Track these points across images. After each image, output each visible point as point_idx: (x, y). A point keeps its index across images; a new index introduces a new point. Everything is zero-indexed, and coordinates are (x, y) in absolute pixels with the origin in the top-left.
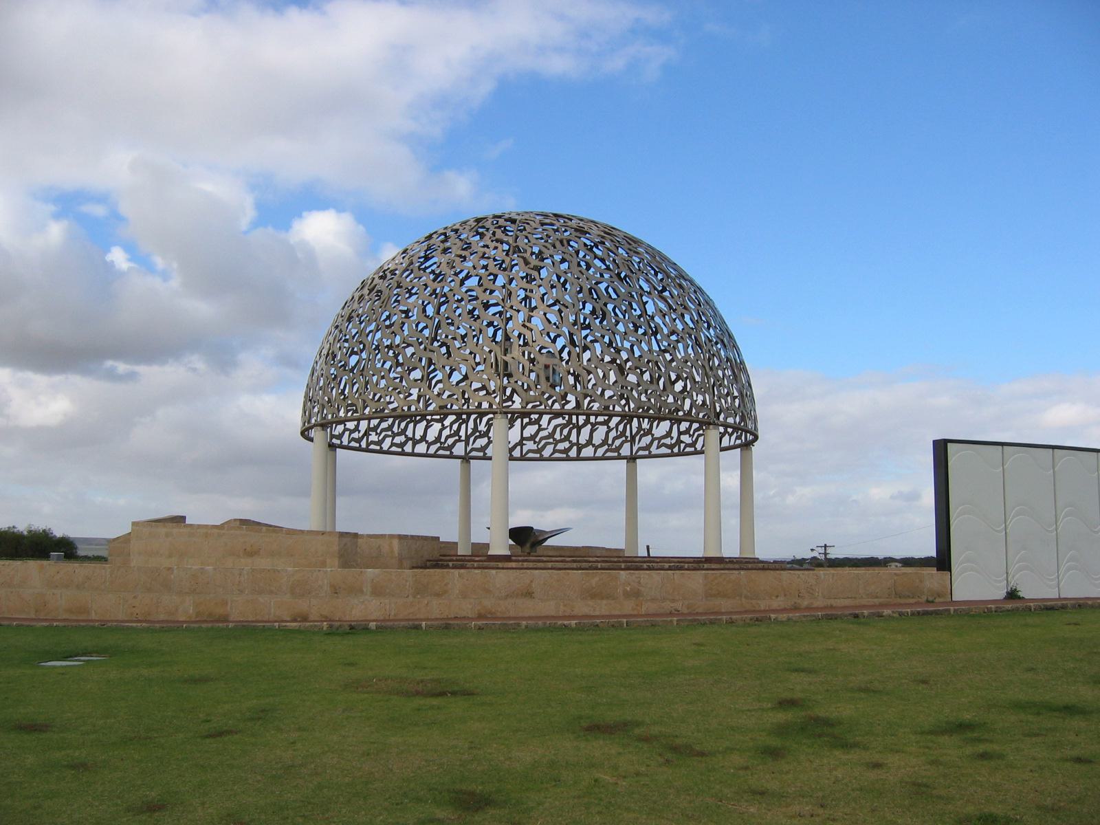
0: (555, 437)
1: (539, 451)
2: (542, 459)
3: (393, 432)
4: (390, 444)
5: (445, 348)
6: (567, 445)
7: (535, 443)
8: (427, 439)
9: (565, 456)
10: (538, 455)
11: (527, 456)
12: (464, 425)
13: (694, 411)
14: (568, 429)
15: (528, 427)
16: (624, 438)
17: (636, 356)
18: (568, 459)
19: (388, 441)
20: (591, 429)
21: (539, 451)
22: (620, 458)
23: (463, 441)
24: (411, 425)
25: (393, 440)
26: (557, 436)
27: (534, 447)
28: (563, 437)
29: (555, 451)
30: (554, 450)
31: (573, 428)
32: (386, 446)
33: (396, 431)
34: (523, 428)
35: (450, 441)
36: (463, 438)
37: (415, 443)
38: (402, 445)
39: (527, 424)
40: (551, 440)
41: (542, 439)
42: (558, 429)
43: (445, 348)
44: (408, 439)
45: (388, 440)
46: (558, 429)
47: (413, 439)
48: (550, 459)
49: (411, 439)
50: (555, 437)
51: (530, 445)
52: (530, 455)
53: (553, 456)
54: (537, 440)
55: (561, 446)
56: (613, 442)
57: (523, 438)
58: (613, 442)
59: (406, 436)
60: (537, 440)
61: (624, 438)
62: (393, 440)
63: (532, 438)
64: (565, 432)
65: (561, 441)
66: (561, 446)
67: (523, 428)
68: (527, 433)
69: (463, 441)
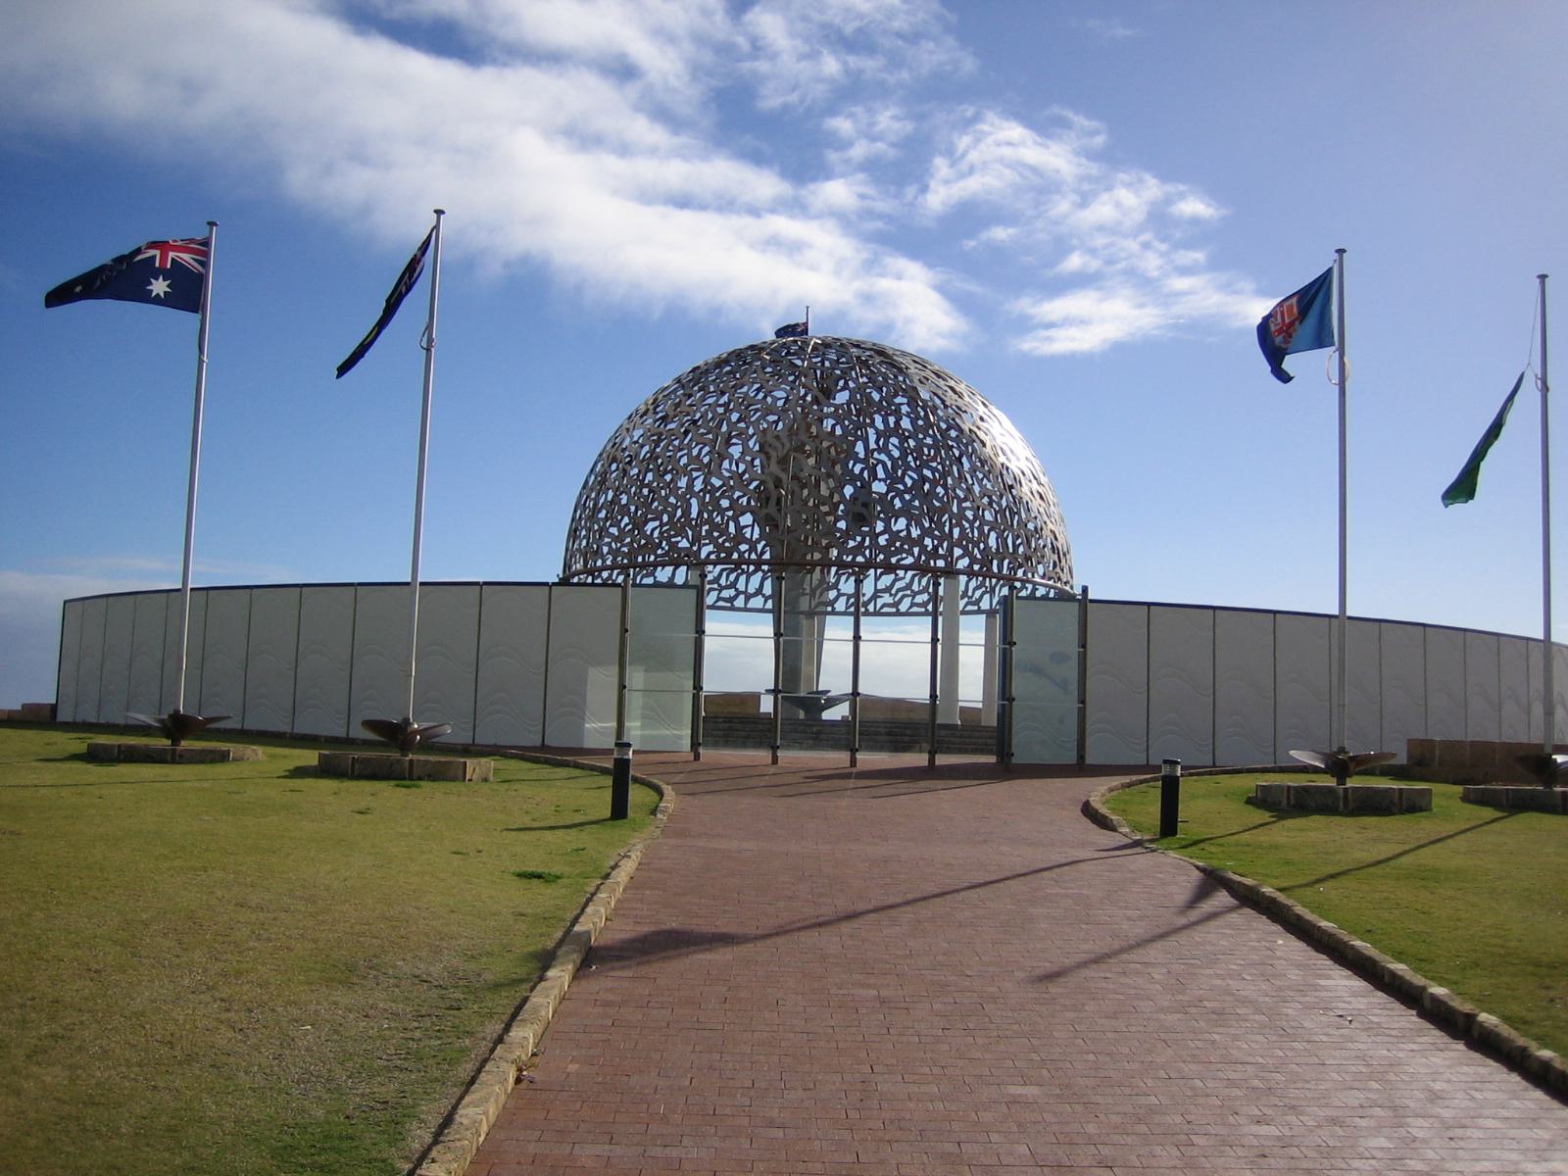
0: (913, 588)
1: (896, 605)
2: (898, 614)
3: (719, 585)
4: (909, 604)
5: (986, 498)
6: (732, 592)
7: (891, 595)
8: (764, 592)
9: (729, 605)
10: (894, 610)
11: (882, 611)
12: (809, 576)
13: (923, 558)
14: (735, 573)
15: (883, 577)
16: (984, 589)
17: (835, 501)
18: (733, 609)
19: (907, 602)
20: (762, 577)
21: (896, 605)
22: (979, 612)
23: (807, 594)
24: (743, 578)
25: (913, 599)
26: (723, 582)
27: (890, 600)
28: (729, 583)
29: (913, 604)
30: (718, 597)
31: (742, 574)
32: (903, 607)
33: (724, 584)
34: (877, 579)
35: (978, 594)
36: (808, 591)
37: (748, 597)
38: (731, 600)
39: (882, 574)
40: (909, 592)
41: (898, 591)
42: (725, 574)
43: (986, 498)
44: (739, 593)
45: (907, 602)
46: (725, 574)
47: (745, 593)
48: (907, 614)
49: (742, 593)
50: (913, 588)
51: (887, 599)
52: (885, 610)
53: (911, 610)
54: (893, 591)
55: (725, 594)
56: (617, 578)
57: (877, 591)
58: (617, 578)
59: (736, 590)
60: (893, 591)
61: (984, 589)
62: (913, 599)
63: (888, 590)
64: (732, 577)
65: (727, 587)
66: (725, 594)
67: (877, 579)
68: (881, 585)
69: (807, 594)
